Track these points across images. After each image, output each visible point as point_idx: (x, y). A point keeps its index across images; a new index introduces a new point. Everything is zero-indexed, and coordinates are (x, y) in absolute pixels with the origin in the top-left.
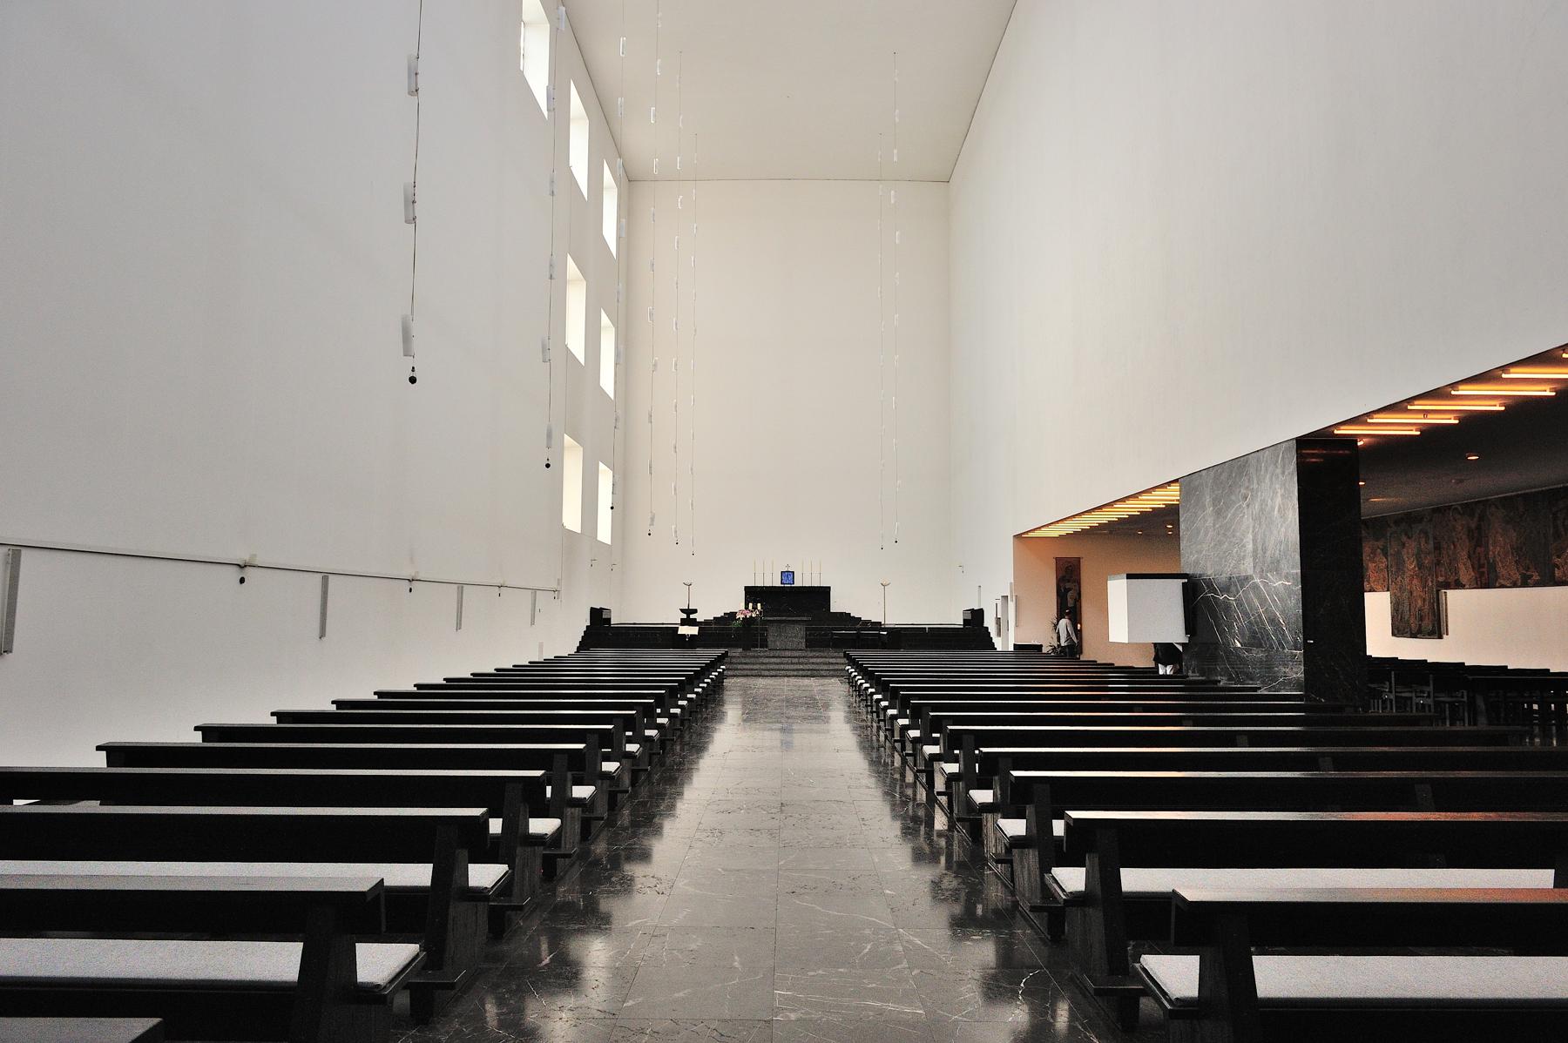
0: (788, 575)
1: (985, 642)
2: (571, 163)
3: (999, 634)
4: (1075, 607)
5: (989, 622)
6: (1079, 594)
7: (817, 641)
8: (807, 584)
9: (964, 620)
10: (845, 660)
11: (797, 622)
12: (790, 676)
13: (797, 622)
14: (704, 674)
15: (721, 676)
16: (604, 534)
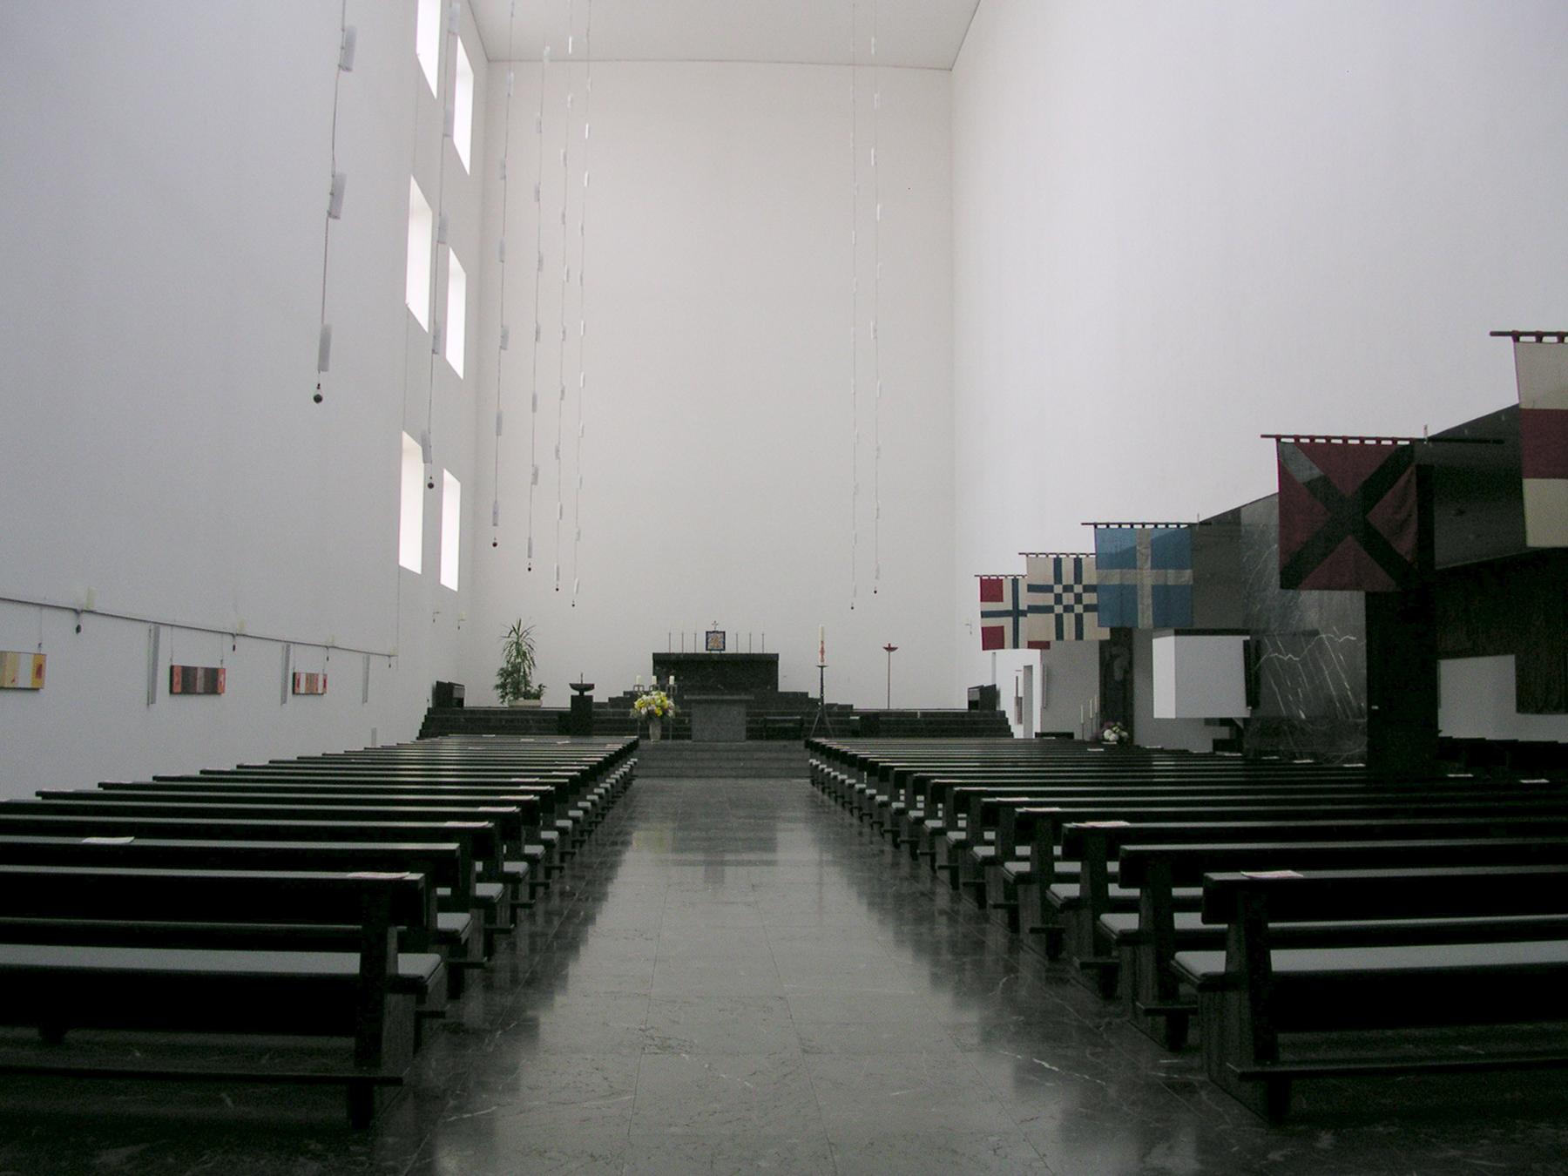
0: (715, 636)
1: (1000, 727)
2: (419, 50)
3: (1020, 720)
4: (1125, 680)
5: (1007, 705)
6: (1131, 663)
7: (761, 731)
8: (744, 650)
9: (970, 703)
10: (808, 753)
11: (734, 702)
12: (725, 777)
13: (734, 702)
14: (585, 785)
15: (627, 780)
16: (450, 577)
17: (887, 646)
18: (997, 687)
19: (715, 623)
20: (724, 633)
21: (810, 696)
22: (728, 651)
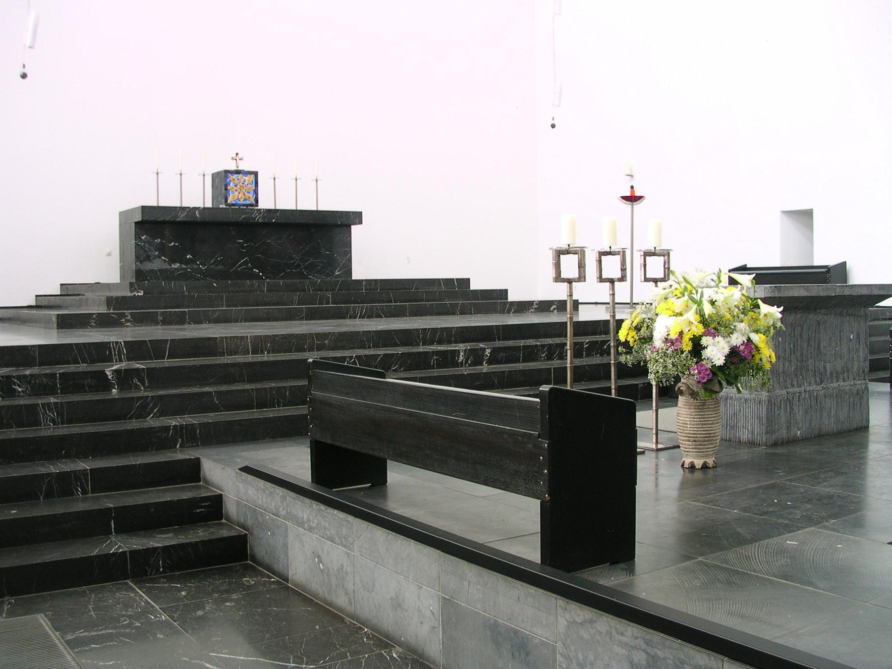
8: (286, 204)
17: (628, 193)
18: (600, 251)
19: (236, 157)
20: (256, 174)
21: (473, 286)
22: (265, 203)
